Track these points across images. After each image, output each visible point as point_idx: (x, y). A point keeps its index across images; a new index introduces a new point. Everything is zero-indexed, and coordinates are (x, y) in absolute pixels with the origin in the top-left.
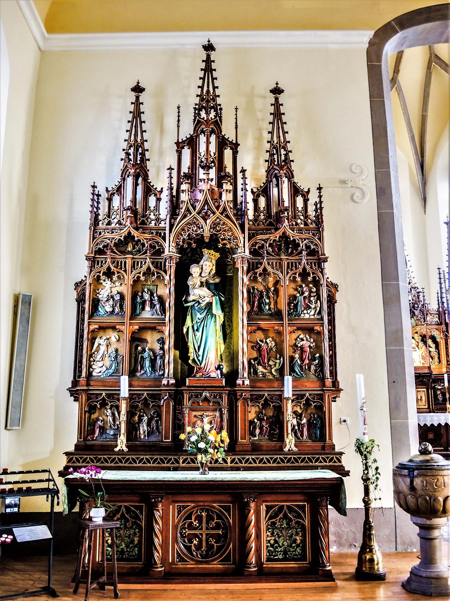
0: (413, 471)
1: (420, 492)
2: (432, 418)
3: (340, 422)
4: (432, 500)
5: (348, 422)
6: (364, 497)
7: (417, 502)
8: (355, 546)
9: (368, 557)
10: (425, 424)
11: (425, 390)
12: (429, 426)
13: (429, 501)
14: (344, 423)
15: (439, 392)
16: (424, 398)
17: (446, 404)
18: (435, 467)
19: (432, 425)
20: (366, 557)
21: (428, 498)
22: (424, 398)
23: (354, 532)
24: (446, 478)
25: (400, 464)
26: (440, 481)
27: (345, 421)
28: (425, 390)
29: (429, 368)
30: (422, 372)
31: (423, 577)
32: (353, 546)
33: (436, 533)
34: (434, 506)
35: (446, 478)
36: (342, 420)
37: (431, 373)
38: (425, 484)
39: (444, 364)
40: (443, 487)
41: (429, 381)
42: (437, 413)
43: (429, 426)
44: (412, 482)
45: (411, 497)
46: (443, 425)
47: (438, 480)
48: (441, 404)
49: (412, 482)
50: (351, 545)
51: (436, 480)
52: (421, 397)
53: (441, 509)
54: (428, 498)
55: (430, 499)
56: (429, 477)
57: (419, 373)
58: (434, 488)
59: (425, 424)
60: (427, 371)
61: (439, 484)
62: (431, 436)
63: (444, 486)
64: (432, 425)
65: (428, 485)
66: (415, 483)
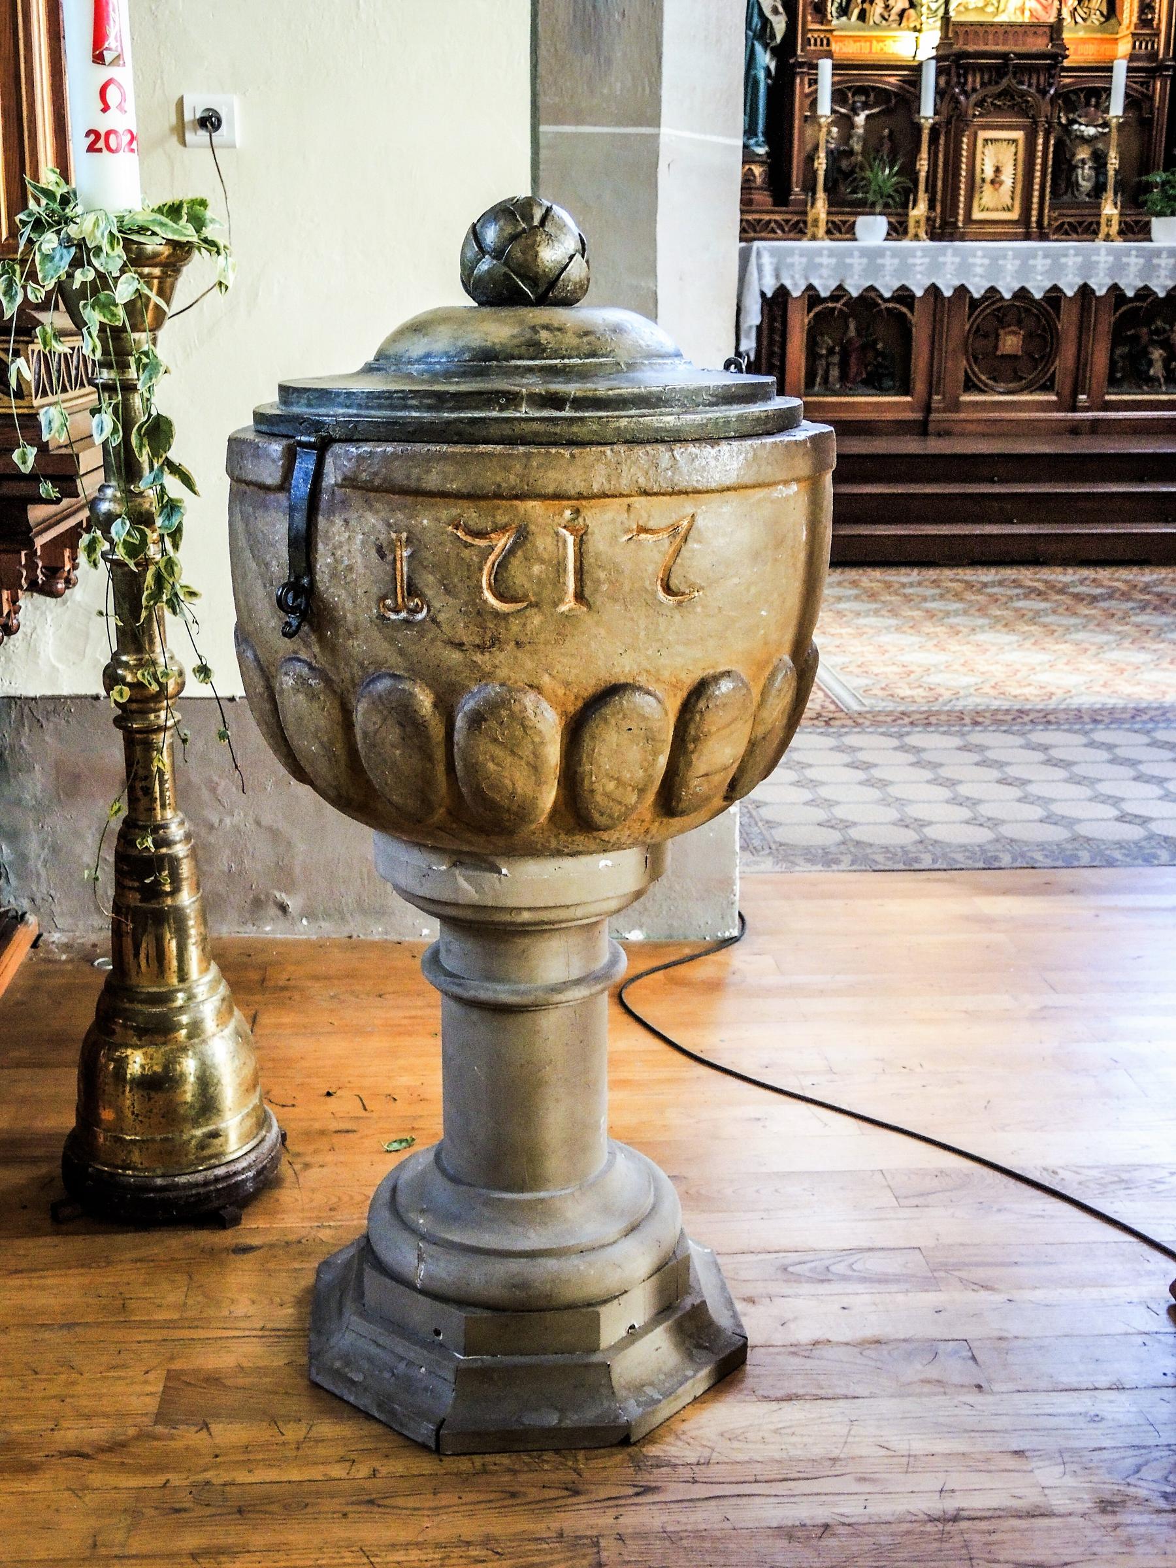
0: (322, 447)
1: (365, 644)
2: (1024, 264)
3: (180, 130)
4: (460, 722)
5: (233, 130)
6: (115, 656)
7: (347, 724)
8: (283, 908)
9: (137, 1062)
10: (993, 290)
11: (1019, 135)
12: (1007, 296)
13: (437, 731)
14: (203, 135)
15: (1083, 153)
16: (1007, 177)
17: (1098, 206)
18: (524, 411)
19: (1022, 294)
20: (122, 1063)
21: (425, 700)
22: (1007, 177)
23: (274, 834)
24: (603, 521)
25: (287, 392)
26: (542, 543)
27: (210, 122)
28: (1019, 135)
29: (1055, 30)
30: (1018, 49)
31: (409, 1285)
32: (273, 911)
33: (552, 963)
34: (473, 768)
35: (603, 521)
36: (188, 116)
37: (1057, 56)
38: (403, 568)
39: (1126, 22)
40: (568, 604)
41: (1044, 93)
42: (1057, 240)
43: (1007, 296)
44: (303, 545)
45: (301, 680)
46: (1070, 293)
47: (523, 536)
48: (1080, 205)
49: (303, 545)
50: (258, 903)
51: (503, 542)
52: (998, 170)
53: (549, 796)
54: (425, 700)
55: (446, 707)
56: (448, 512)
57: (1005, 56)
58: (481, 613)
59: (993, 290)
60: (1040, 44)
61: (520, 575)
62: (1011, 343)
63: (579, 596)
64: (1022, 294)
65: (428, 581)
66: (323, 560)
